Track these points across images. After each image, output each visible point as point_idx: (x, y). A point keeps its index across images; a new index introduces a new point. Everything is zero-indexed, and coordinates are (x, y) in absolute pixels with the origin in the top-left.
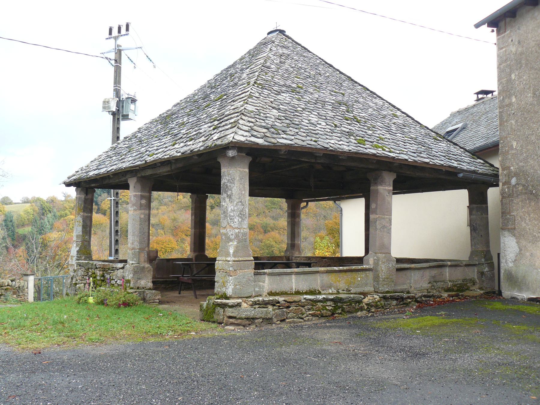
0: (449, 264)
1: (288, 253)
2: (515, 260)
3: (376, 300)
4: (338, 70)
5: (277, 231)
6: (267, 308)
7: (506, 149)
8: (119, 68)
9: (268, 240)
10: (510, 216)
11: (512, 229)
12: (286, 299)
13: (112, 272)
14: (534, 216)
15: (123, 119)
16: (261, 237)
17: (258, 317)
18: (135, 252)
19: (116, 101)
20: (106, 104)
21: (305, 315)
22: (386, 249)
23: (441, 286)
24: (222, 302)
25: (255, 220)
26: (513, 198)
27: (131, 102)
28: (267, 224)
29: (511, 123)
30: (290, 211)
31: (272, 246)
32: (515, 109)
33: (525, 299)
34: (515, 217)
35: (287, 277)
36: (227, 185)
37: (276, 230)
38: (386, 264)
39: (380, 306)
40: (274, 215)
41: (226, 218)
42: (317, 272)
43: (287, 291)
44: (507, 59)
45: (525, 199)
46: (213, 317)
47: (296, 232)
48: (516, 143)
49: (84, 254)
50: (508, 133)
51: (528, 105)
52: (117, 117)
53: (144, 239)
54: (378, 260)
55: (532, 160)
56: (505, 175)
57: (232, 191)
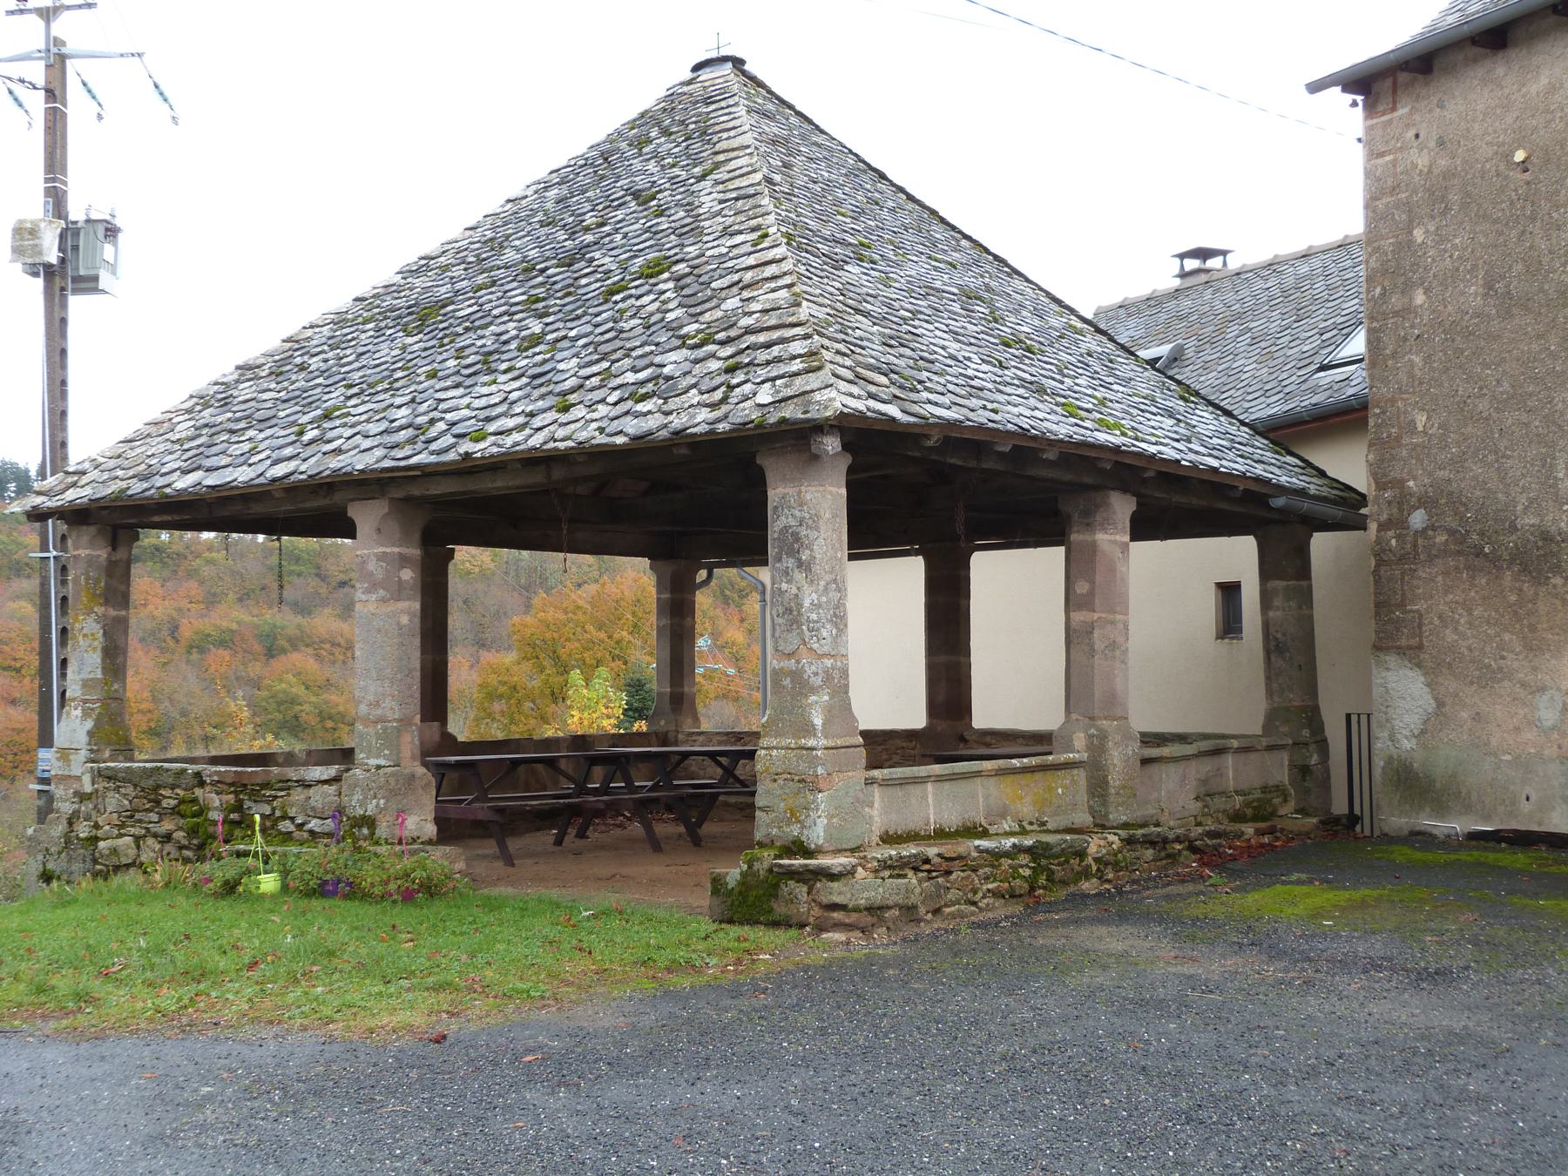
0: (1236, 746)
1: (662, 723)
2: (1423, 732)
3: (1114, 846)
4: (901, 190)
5: (310, 650)
6: (904, 876)
7: (1393, 431)
8: (61, 117)
9: (281, 680)
10: (1405, 612)
11: (1410, 648)
12: (942, 850)
13: (283, 793)
14: (1486, 614)
15: (76, 291)
16: (255, 669)
17: (890, 903)
18: (385, 729)
19: (59, 230)
20: (24, 235)
21: (980, 894)
22: (1113, 704)
23: (1222, 807)
24: (806, 865)
25: (235, 614)
26: (1416, 564)
27: (106, 237)
28: (275, 626)
29: (1410, 360)
30: (666, 596)
31: (294, 701)
32: (1425, 325)
33: (1457, 835)
34: (1421, 615)
35: (915, 790)
36: (798, 533)
37: (307, 646)
38: (1120, 749)
39: (1123, 864)
40: (300, 599)
41: (794, 627)
42: (978, 774)
43: (918, 829)
44: (1398, 186)
45: (1457, 568)
46: (771, 911)
47: (686, 660)
48: (1424, 418)
49: (109, 743)
50: (1400, 389)
51: (1467, 317)
52: (58, 281)
53: (410, 688)
54: (1103, 737)
55: (1479, 465)
56: (1390, 503)
57: (812, 550)
